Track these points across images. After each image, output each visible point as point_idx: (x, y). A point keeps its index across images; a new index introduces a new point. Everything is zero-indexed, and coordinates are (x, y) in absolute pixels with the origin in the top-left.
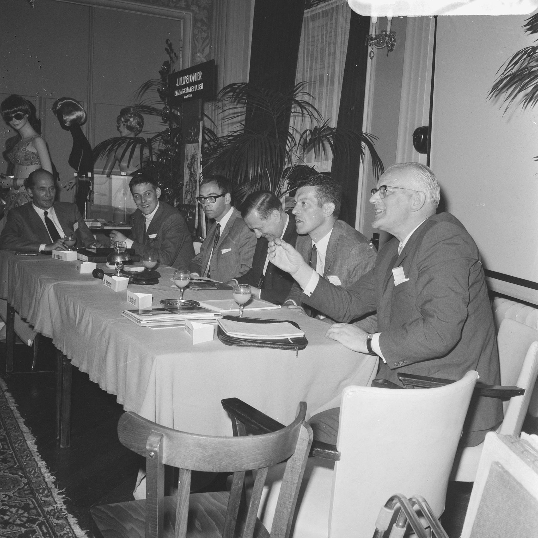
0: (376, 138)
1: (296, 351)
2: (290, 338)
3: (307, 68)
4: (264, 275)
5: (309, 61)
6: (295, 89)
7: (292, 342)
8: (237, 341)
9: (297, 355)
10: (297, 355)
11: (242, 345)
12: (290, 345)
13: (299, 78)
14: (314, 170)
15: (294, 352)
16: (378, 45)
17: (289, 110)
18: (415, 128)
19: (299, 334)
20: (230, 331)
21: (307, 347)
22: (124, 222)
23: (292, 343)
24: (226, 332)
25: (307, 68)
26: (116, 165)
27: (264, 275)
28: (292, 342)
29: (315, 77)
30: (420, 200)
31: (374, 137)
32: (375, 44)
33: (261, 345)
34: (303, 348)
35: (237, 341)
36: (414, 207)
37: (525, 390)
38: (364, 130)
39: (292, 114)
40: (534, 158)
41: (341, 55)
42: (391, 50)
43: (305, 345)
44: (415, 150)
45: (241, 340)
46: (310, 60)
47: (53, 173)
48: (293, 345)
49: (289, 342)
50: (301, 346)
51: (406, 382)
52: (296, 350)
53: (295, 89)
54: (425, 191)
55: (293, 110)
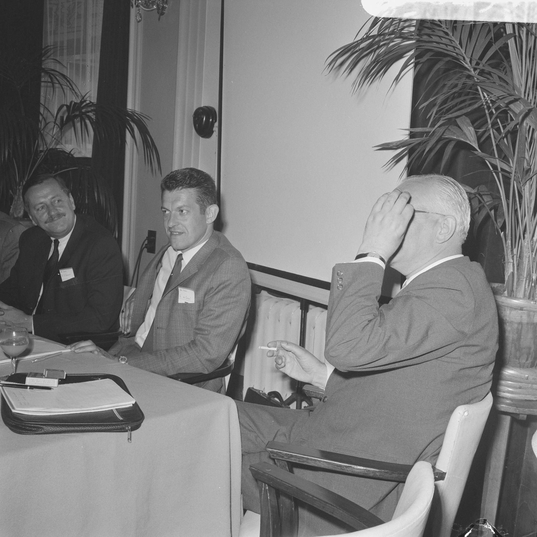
0: (148, 118)
1: (127, 433)
2: (116, 409)
3: (51, 31)
4: (230, 375)
5: (53, 23)
6: (43, 52)
7: (121, 419)
8: (34, 427)
9: (130, 439)
10: (130, 439)
11: (43, 431)
12: (119, 425)
13: (49, 40)
14: (72, 155)
15: (126, 435)
16: (147, 7)
17: (40, 77)
18: (195, 109)
19: (127, 402)
20: (21, 405)
21: (144, 424)
22: (481, 526)
23: (122, 421)
24: (14, 408)
25: (51, 31)
26: (486, 89)
27: (230, 375)
28: (121, 419)
29: (62, 42)
30: (449, 228)
31: (146, 117)
32: (142, 5)
33: (73, 429)
34: (136, 427)
35: (34, 427)
36: (441, 237)
37: (446, 473)
38: (130, 106)
39: (43, 84)
40: (375, 147)
41: (93, 17)
42: (162, 14)
43: (141, 421)
44: (196, 133)
45: (42, 425)
46: (53, 21)
47: (125, 129)
48: (123, 424)
49: (118, 420)
50: (135, 424)
51: (275, 455)
52: (127, 431)
53: (43, 52)
54: (454, 214)
55: (43, 79)
